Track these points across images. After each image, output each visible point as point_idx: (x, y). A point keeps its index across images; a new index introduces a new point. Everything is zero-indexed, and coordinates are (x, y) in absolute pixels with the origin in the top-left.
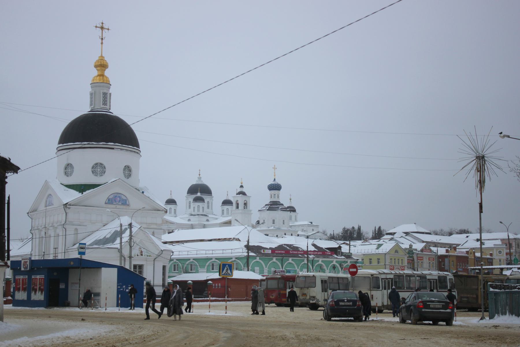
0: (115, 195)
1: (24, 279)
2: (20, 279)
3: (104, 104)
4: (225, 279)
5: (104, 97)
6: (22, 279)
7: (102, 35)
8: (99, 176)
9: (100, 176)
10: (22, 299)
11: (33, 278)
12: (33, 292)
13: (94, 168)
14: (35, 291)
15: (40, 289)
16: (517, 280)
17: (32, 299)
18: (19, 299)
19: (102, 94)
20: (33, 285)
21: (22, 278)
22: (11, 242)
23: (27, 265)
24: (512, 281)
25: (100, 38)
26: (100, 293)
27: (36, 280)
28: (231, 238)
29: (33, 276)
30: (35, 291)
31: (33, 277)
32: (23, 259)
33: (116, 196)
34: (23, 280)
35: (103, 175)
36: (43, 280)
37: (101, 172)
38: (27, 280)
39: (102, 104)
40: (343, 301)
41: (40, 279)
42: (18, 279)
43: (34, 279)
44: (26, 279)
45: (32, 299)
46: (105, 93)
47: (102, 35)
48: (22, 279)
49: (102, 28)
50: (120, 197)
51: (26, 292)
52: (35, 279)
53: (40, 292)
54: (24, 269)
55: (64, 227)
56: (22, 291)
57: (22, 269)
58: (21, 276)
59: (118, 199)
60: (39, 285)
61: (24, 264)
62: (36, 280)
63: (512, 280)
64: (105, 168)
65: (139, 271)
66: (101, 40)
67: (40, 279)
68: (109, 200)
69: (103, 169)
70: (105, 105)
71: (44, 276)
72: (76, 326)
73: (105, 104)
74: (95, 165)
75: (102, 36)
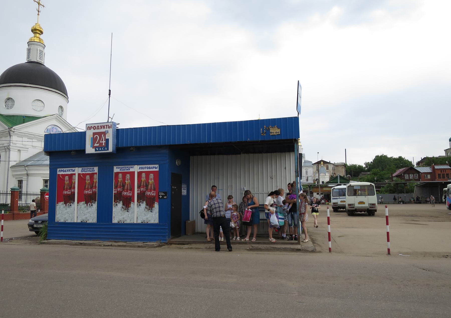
0: (53, 126)
1: (85, 175)
2: (71, 176)
4: (13, 191)
6: (79, 175)
7: (39, 8)
10: (79, 221)
11: (117, 174)
12: (120, 205)
14: (127, 202)
15: (141, 197)
16: (360, 187)
17: (115, 221)
18: (69, 221)
20: (116, 187)
21: (80, 172)
23: (107, 141)
24: (355, 187)
25: (37, 10)
26: (345, 207)
27: (128, 176)
29: (115, 167)
30: (127, 202)
31: (116, 170)
32: (89, 128)
33: (53, 128)
34: (82, 178)
36: (152, 176)
38: (96, 177)
41: (144, 175)
42: (64, 176)
43: (120, 175)
44: (92, 175)
45: (115, 221)
47: (39, 8)
48: (79, 175)
49: (39, 4)
50: (56, 129)
51: (95, 206)
52: (124, 174)
53: (144, 205)
54: (96, 150)
56: (78, 203)
57: (89, 150)
58: (77, 169)
59: (55, 130)
60: (139, 187)
61: (94, 140)
62: (128, 176)
63: (354, 187)
65: (47, 183)
66: (38, 12)
67: (144, 175)
68: (47, 130)
71: (157, 166)
75: (39, 9)
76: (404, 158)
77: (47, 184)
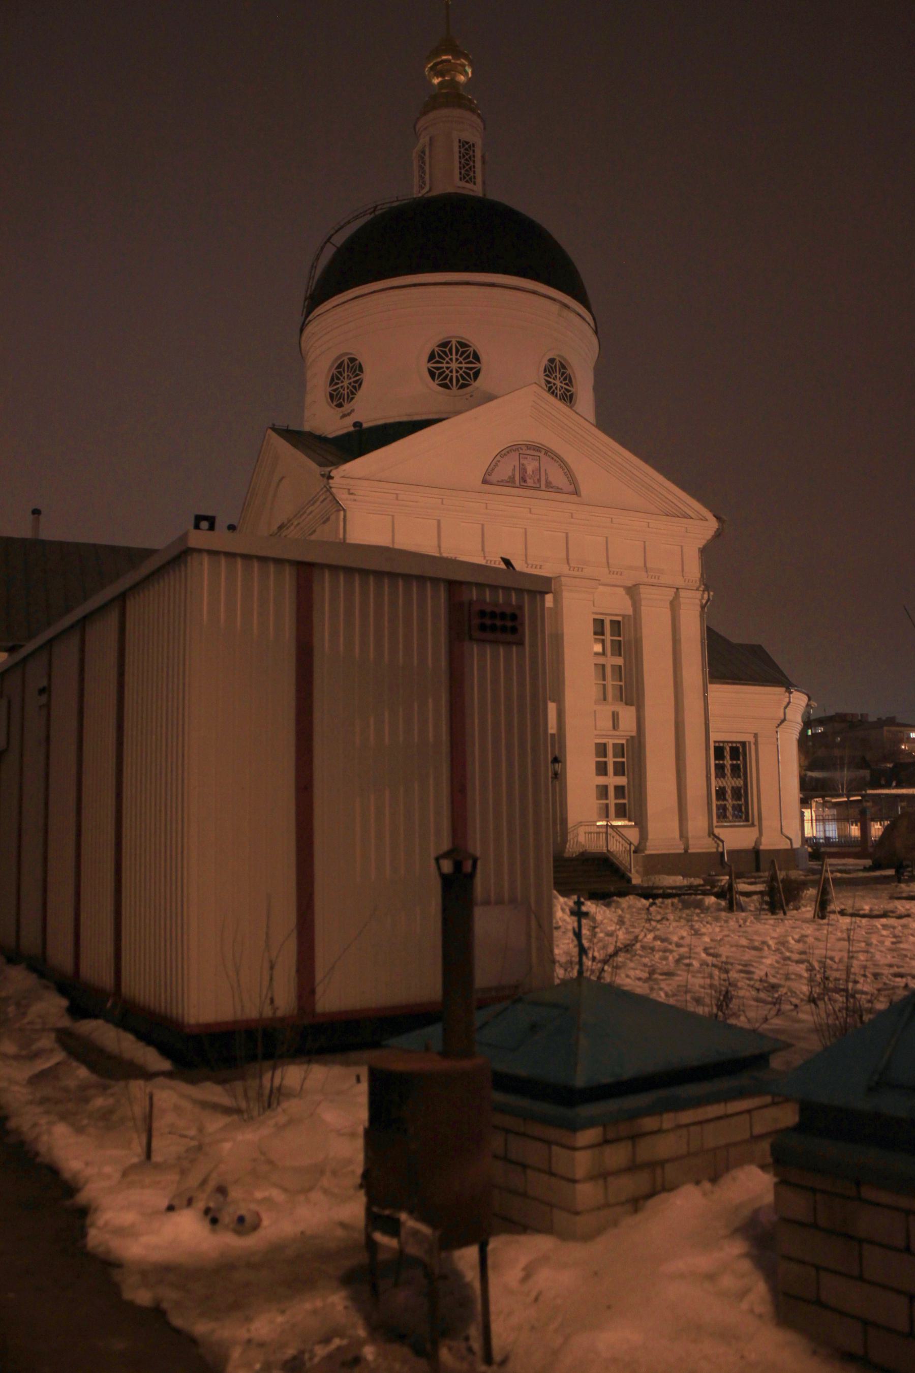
3: (465, 178)
5: (464, 156)
8: (454, 388)
9: (450, 342)
13: (447, 381)
19: (456, 145)
22: (760, 747)
28: (148, 553)
35: (471, 349)
37: (461, 359)
39: (457, 176)
40: (832, 838)
46: (467, 143)
55: (788, 841)
64: (477, 358)
69: (471, 362)
70: (467, 182)
72: (312, 1114)
73: (467, 178)
74: (439, 346)
76: (507, 562)
77: (717, 762)
